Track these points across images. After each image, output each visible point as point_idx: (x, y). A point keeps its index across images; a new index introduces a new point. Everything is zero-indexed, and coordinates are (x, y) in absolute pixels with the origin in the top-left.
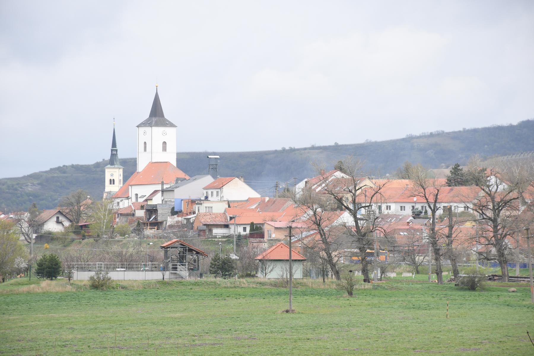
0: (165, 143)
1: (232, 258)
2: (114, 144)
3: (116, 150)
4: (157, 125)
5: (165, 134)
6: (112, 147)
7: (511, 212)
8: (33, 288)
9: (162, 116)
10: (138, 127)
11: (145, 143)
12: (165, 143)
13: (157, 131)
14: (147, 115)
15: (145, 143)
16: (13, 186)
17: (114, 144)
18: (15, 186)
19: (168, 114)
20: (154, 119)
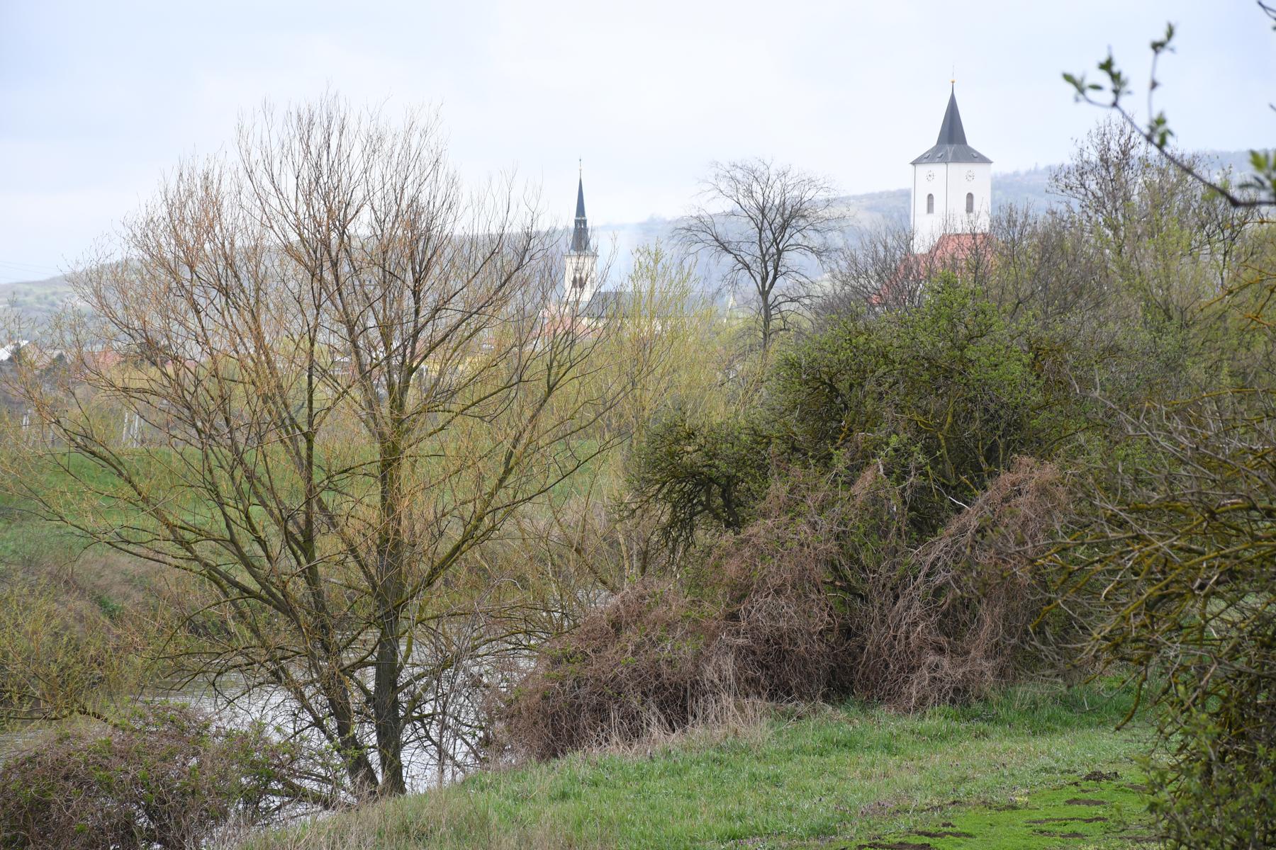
0: (970, 196)
1: (835, 461)
2: (581, 209)
3: (585, 222)
4: (957, 159)
5: (970, 177)
6: (577, 215)
7: (318, 490)
8: (221, 477)
9: (963, 140)
10: (914, 163)
11: (930, 197)
12: (970, 196)
13: (958, 170)
14: (933, 141)
15: (930, 197)
16: (46, 298)
17: (581, 209)
18: (51, 298)
19: (973, 139)
20: (950, 149)
